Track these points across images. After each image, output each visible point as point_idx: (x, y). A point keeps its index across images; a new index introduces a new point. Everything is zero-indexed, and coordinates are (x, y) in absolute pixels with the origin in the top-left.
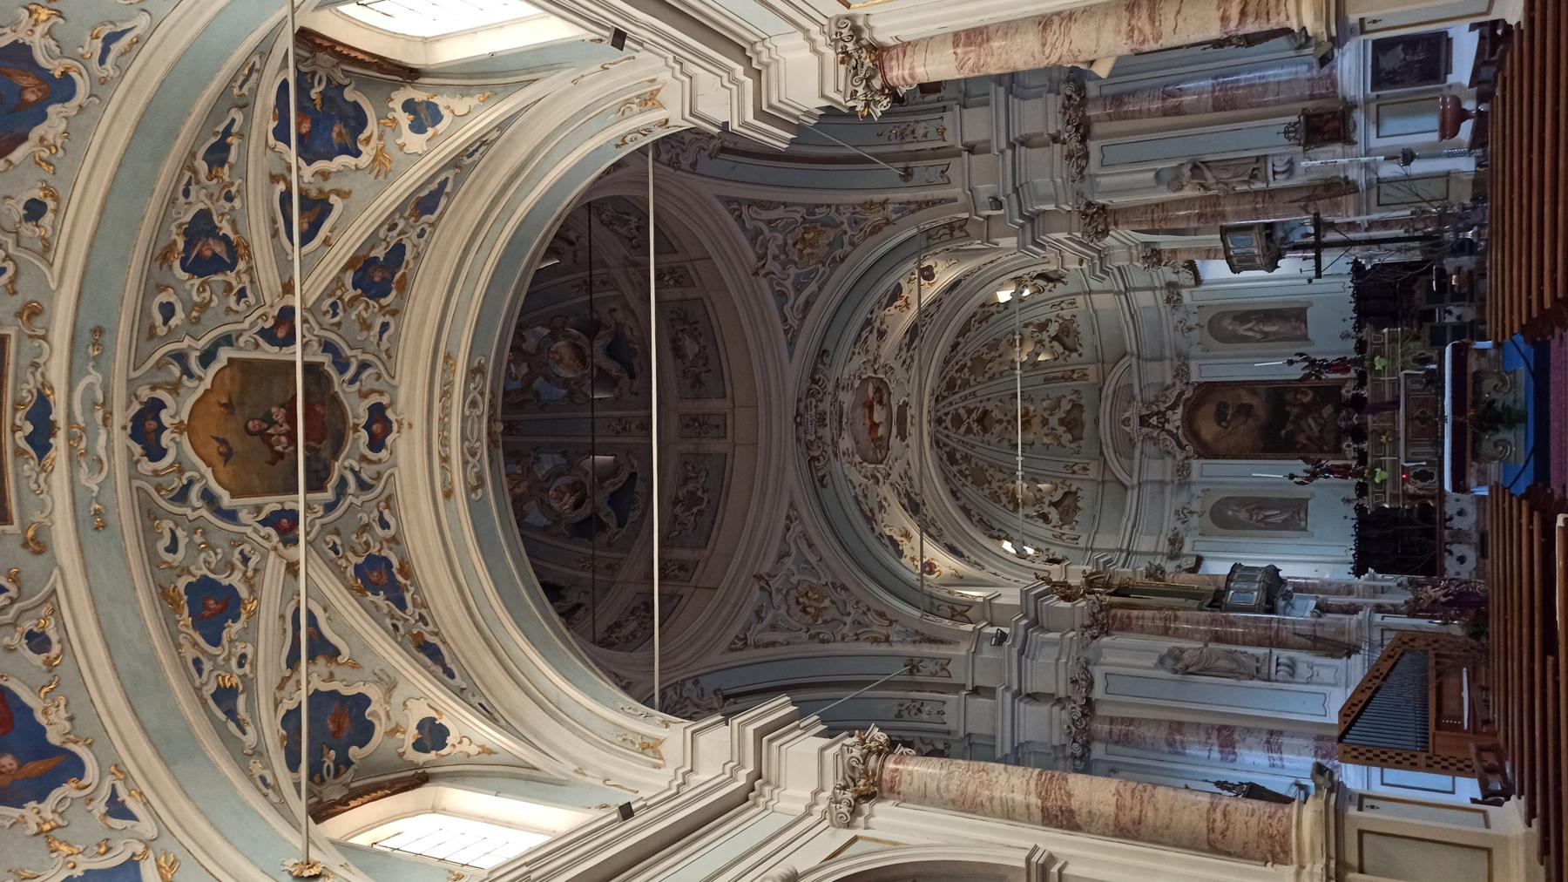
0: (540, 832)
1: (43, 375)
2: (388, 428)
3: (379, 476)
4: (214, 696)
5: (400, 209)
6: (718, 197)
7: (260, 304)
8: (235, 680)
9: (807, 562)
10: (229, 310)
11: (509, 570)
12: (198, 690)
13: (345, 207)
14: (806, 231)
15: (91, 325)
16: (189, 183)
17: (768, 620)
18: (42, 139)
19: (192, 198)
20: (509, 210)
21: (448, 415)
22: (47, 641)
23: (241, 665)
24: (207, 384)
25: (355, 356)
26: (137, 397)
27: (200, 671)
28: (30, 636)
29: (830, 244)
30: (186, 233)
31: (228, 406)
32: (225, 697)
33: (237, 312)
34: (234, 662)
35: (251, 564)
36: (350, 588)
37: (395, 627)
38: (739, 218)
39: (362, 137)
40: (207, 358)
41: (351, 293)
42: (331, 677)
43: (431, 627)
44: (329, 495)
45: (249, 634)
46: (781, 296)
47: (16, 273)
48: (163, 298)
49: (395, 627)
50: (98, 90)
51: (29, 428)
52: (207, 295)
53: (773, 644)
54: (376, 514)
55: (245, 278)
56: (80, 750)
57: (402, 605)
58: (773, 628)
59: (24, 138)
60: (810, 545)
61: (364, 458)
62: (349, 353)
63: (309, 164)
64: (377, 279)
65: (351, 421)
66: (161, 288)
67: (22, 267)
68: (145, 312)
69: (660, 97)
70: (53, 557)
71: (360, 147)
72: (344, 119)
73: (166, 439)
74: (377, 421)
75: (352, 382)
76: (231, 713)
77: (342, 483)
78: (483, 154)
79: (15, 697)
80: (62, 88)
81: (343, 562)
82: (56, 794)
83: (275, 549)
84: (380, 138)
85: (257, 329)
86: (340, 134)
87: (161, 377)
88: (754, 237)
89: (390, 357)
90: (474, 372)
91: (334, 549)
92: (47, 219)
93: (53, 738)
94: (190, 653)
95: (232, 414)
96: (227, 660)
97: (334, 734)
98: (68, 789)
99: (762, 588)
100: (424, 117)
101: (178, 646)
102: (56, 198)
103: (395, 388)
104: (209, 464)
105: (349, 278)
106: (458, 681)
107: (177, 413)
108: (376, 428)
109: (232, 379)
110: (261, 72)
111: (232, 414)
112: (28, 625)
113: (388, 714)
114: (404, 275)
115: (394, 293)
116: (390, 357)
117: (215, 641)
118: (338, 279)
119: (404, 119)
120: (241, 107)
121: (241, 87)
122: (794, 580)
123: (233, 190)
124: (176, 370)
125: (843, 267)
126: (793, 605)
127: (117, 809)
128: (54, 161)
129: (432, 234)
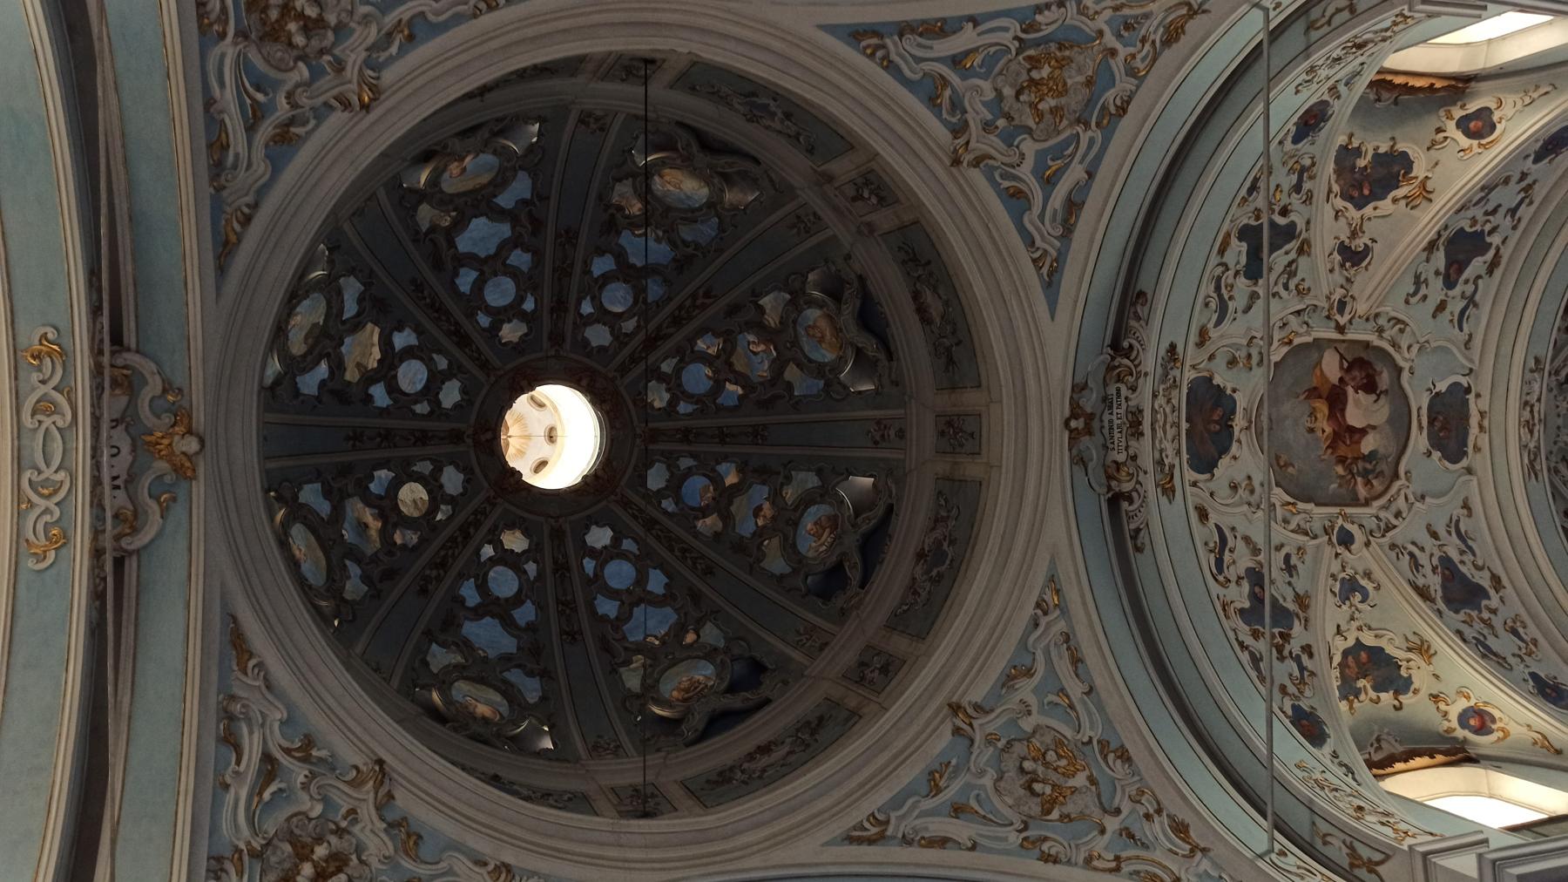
0: (1540, 811)
6: (822, 27)
9: (1062, 691)
14: (1035, 63)
17: (951, 792)
29: (1089, 83)
38: (889, 66)
46: (1016, 199)
53: (943, 842)
58: (958, 810)
60: (1076, 660)
88: (932, 92)
99: (957, 731)
100: (1480, 126)
122: (1027, 725)
125: (1127, 123)
126: (1012, 774)
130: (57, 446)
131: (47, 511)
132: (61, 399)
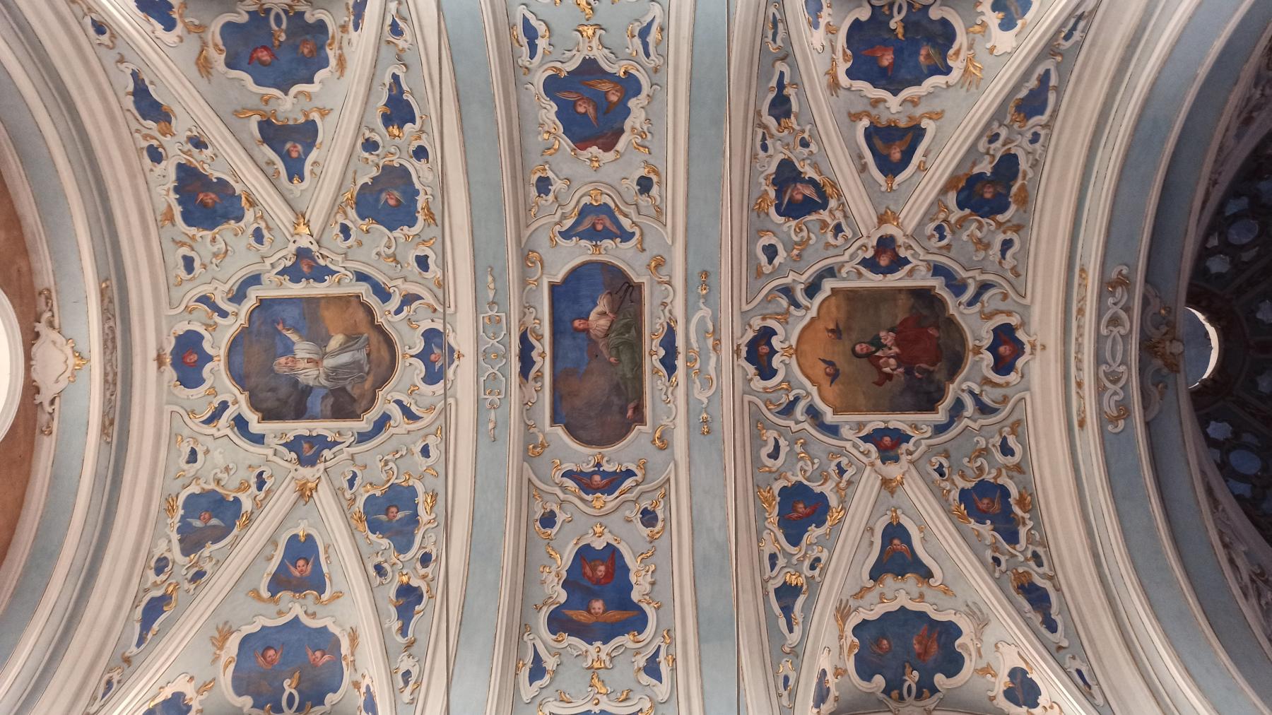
1: (670, 312)
2: (1018, 349)
3: (1005, 399)
4: (777, 591)
5: (998, 116)
7: (857, 236)
8: (801, 580)
10: (828, 245)
11: (1151, 518)
12: (765, 582)
13: (938, 130)
15: (698, 270)
16: (764, 138)
18: (633, 128)
19: (771, 151)
20: (1131, 89)
21: (1081, 335)
22: (656, 518)
23: (813, 567)
24: (813, 313)
25: (972, 279)
26: (750, 326)
27: (773, 566)
28: (645, 512)
30: (774, 183)
31: (836, 332)
33: (837, 246)
34: (807, 563)
35: (846, 476)
36: (948, 512)
37: (997, 561)
39: (951, 52)
40: (812, 290)
42: (922, 597)
43: (1045, 569)
44: (940, 416)
45: (828, 542)
47: (642, 234)
49: (997, 561)
50: (656, 79)
51: (662, 352)
52: (805, 234)
54: (997, 440)
55: (839, 214)
56: (650, 611)
57: (1012, 538)
59: (622, 131)
62: (964, 274)
63: (895, 94)
64: (988, 196)
65: (971, 343)
66: (761, 232)
67: (646, 231)
68: (751, 255)
70: (673, 453)
71: (950, 63)
72: (931, 39)
73: (776, 362)
74: (1005, 343)
75: (970, 304)
76: (787, 610)
77: (958, 406)
78: (1086, 31)
79: (621, 557)
80: (630, 86)
81: (947, 485)
83: (872, 465)
84: (970, 47)
85: (858, 260)
86: (928, 56)
87: (771, 308)
89: (1017, 275)
90: (1108, 286)
92: (655, 191)
93: (635, 596)
94: (768, 548)
95: (840, 338)
96: (800, 561)
97: (919, 655)
98: (626, 640)
101: (760, 540)
102: (657, 173)
103: (1027, 307)
104: (813, 383)
105: (951, 199)
106: (1059, 637)
107: (786, 339)
108: (1003, 349)
109: (838, 307)
110: (784, 21)
111: (840, 338)
112: (645, 503)
113: (979, 651)
114: (1023, 187)
115: (1013, 208)
116: (1017, 275)
117: (795, 540)
118: (938, 203)
120: (783, 59)
121: (774, 40)
123: (806, 135)
124: (784, 302)
127: (652, 669)
128: (647, 144)
130: (1120, 348)
131: (1115, 393)
132: (1123, 315)
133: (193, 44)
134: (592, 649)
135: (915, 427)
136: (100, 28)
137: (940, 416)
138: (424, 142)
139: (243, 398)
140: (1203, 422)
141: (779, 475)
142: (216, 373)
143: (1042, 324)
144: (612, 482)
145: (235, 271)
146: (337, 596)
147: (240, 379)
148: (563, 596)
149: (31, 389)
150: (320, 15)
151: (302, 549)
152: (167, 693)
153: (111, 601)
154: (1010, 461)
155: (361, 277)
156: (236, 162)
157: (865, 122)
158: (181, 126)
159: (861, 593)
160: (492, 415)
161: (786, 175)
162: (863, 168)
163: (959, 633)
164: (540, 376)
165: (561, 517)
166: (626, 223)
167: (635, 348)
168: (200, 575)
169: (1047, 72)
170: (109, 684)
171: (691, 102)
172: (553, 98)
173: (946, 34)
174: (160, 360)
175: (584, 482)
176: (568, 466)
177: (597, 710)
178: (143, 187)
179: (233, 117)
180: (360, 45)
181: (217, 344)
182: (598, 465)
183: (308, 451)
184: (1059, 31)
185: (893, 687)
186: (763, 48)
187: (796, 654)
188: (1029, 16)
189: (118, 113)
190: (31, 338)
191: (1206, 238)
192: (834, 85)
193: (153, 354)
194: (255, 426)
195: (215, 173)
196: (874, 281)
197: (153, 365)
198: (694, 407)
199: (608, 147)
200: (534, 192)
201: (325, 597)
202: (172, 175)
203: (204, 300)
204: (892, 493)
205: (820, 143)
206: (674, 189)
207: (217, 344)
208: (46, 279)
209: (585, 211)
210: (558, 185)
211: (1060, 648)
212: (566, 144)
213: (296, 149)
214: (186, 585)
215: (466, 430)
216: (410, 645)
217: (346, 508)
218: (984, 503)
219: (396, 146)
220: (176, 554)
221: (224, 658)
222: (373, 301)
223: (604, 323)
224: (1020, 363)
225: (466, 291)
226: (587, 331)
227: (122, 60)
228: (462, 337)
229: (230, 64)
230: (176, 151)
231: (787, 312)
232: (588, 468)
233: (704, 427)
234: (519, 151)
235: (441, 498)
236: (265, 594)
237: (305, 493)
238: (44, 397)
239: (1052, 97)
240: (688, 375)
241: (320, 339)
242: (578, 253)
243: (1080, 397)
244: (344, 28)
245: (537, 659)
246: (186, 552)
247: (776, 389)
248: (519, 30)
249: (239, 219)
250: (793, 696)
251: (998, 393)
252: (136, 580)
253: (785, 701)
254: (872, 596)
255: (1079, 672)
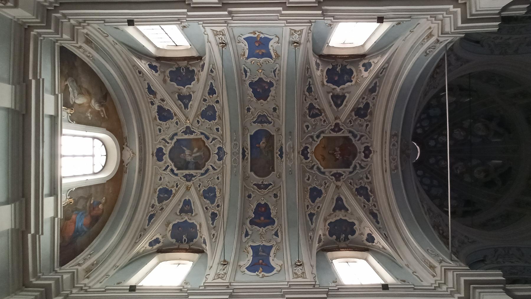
2: (370, 152)
3: (367, 165)
4: (309, 215)
5: (364, 93)
10: (322, 125)
12: (306, 212)
23: (318, 208)
24: (318, 143)
28: (275, 194)
30: (308, 109)
32: (311, 215)
34: (316, 208)
36: (353, 194)
37: (364, 206)
40: (318, 137)
41: (354, 117)
42: (345, 216)
44: (351, 169)
45: (322, 202)
48: (306, 124)
49: (364, 206)
51: (279, 153)
54: (365, 175)
55: (325, 117)
57: (368, 200)
61: (362, 160)
62: (356, 133)
65: (358, 150)
66: (305, 122)
68: (302, 128)
69: (433, 33)
75: (358, 140)
76: (311, 220)
77: (355, 167)
78: (385, 72)
80: (271, 84)
81: (352, 187)
82: (266, 228)
84: (357, 76)
90: (392, 136)
91: (351, 184)
92: (277, 111)
93: (272, 216)
94: (306, 204)
96: (315, 207)
98: (270, 227)
101: (304, 201)
102: (278, 106)
105: (353, 113)
106: (380, 225)
108: (367, 152)
110: (310, 68)
112: (275, 192)
115: (368, 116)
117: (313, 201)
118: (350, 115)
119: (363, 69)
120: (310, 78)
124: (311, 140)
127: (276, 234)
129: (377, 98)
132: (396, 143)
133: (162, 77)
134: (261, 229)
135: (344, 172)
136: (140, 72)
137: (351, 169)
138: (218, 99)
139: (173, 164)
140: (416, 171)
141: (310, 185)
142: (166, 158)
143: (376, 146)
144: (266, 187)
145: (171, 132)
146: (196, 215)
147: (171, 159)
148: (253, 216)
149: (122, 162)
150: (193, 68)
151: (187, 203)
152: (155, 238)
153: (140, 215)
154: (368, 181)
155: (202, 133)
156: (172, 105)
157: (331, 94)
158: (159, 96)
159: (330, 215)
160: (235, 169)
161: (311, 107)
162: (331, 106)
163: (355, 225)
164: (247, 158)
165: (253, 196)
166: (270, 119)
167: (272, 151)
168: (162, 209)
169: (376, 82)
170: (141, 235)
171: (287, 88)
172: (251, 88)
173: (351, 72)
174: (153, 154)
175: (259, 186)
176: (254, 183)
177: (262, 244)
178: (149, 111)
179: (171, 94)
180: (203, 75)
181: (166, 151)
182: (262, 182)
183: (189, 178)
184: (379, 72)
185: (338, 238)
186: (305, 75)
187: (313, 230)
188: (371, 68)
189: (144, 93)
190: (122, 149)
191: (417, 124)
192: (323, 85)
193: (151, 153)
194: (176, 171)
195: (167, 108)
196: (334, 134)
197: (151, 156)
198: (288, 166)
199: (265, 100)
200: (246, 111)
201: (193, 215)
202: (156, 108)
203: (163, 139)
204: (338, 189)
205: (320, 99)
206: (282, 110)
207: (166, 151)
208: (126, 134)
209: (259, 116)
210: (252, 110)
211: (380, 228)
212: (254, 99)
213: (186, 101)
214: (159, 211)
215: (227, 171)
216: (214, 227)
217: (198, 192)
218: (362, 192)
219: (211, 100)
220: (157, 203)
221: (168, 230)
222: (205, 140)
223: (264, 145)
224: (371, 156)
225: (227, 137)
226: (259, 147)
227: (145, 80)
228: (227, 149)
229: (171, 81)
230: (157, 103)
231: (312, 142)
232: (260, 183)
233: (290, 172)
234: (242, 101)
235: (222, 190)
236: (178, 214)
237: (188, 188)
238: (125, 164)
239: (377, 88)
240: (286, 159)
241: (192, 150)
242: (256, 127)
243: (386, 164)
244: (199, 71)
245: (247, 231)
246: (159, 203)
247: (309, 162)
248: (243, 71)
249: (172, 119)
250: (312, 241)
251: (365, 163)
252: (147, 210)
253: (310, 242)
254: (333, 216)
255: (385, 234)
